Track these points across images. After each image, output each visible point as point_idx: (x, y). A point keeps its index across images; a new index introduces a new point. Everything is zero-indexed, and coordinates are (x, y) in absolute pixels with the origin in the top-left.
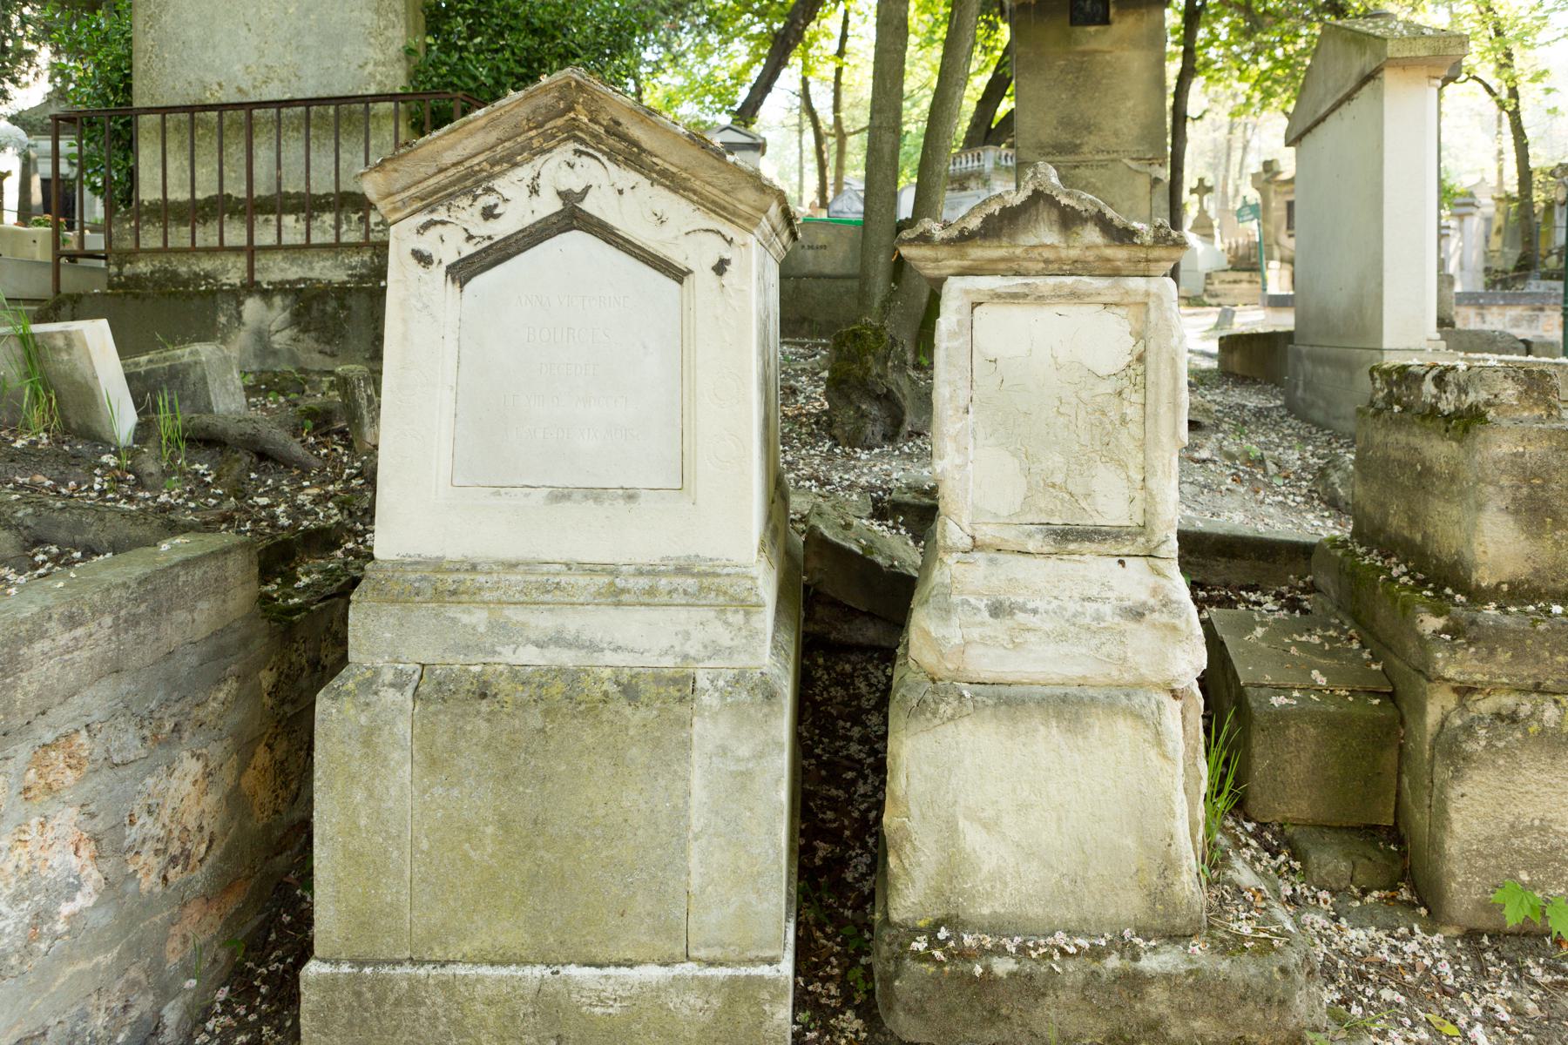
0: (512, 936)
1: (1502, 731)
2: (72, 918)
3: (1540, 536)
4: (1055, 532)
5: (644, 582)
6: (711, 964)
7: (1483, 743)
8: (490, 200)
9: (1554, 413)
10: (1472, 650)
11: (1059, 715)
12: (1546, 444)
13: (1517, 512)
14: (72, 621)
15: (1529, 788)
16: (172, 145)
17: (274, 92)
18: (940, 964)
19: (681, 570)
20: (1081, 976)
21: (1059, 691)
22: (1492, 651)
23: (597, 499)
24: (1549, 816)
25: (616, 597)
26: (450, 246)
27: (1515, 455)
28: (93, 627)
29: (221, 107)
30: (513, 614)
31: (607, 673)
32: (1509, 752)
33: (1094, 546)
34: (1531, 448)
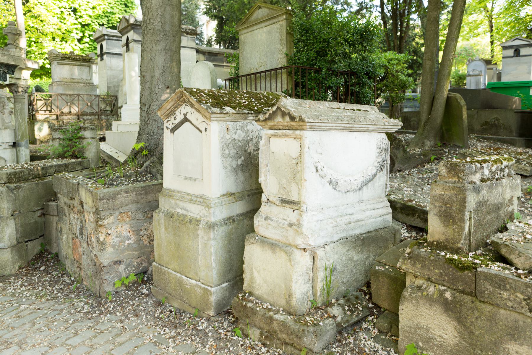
0: (177, 267)
1: (415, 291)
2: (128, 244)
3: (448, 226)
4: (283, 200)
5: (195, 199)
6: (202, 284)
7: (409, 293)
8: (175, 116)
9: (461, 180)
10: (409, 261)
11: (271, 248)
12: (452, 192)
13: (440, 216)
14: (126, 192)
15: (422, 314)
16: (248, 83)
17: (262, 69)
18: (240, 300)
19: (201, 197)
20: (262, 313)
21: (274, 242)
22: (415, 263)
23: (190, 180)
24: (429, 326)
25: (191, 201)
26: (171, 126)
27: (441, 194)
28: (131, 194)
29: (265, 72)
30: (178, 202)
31: (189, 217)
32: (416, 298)
33: (288, 205)
34: (447, 193)
